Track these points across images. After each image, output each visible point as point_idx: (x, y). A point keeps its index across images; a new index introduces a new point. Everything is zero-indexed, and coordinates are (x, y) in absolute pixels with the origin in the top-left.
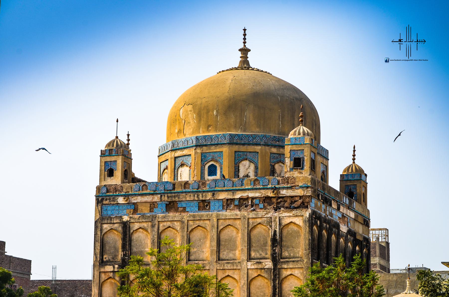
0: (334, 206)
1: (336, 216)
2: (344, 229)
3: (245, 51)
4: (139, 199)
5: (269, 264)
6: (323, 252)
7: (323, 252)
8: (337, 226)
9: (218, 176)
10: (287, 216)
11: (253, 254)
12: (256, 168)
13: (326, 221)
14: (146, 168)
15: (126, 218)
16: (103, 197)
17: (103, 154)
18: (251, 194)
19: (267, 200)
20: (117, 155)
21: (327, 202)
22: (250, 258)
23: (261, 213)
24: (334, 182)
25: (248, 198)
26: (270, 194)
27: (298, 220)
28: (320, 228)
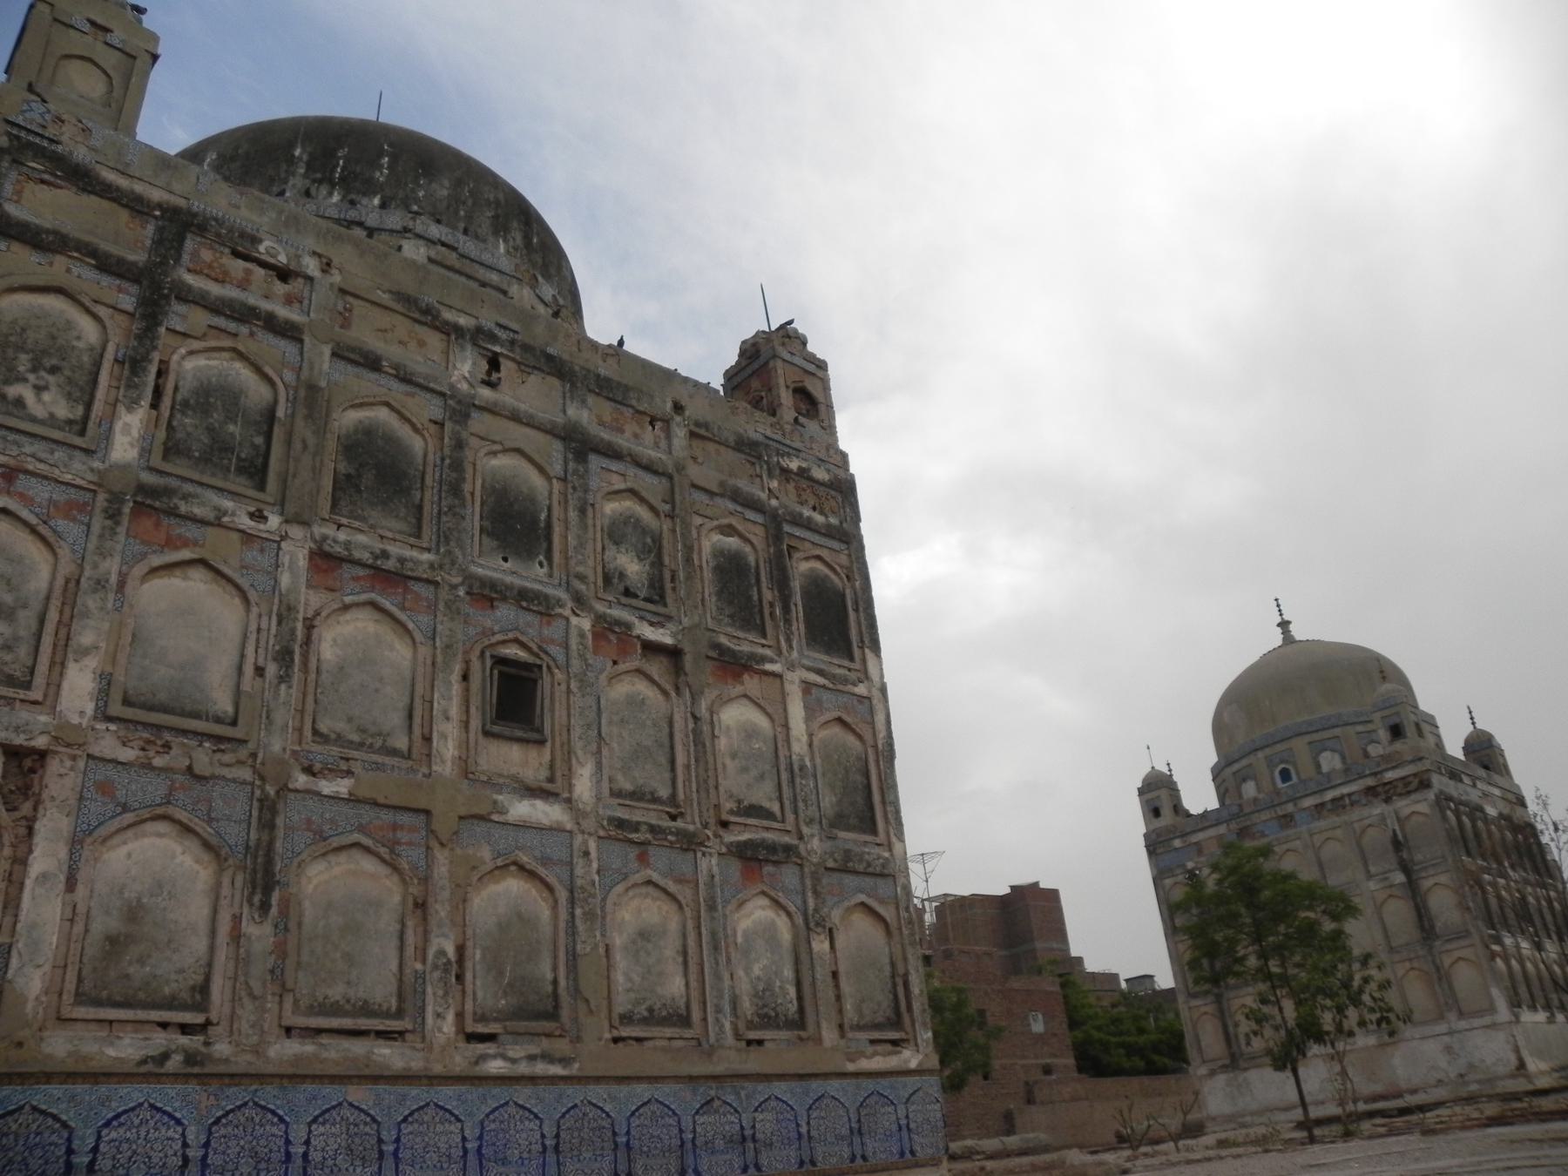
0: (1466, 780)
1: (1474, 796)
2: (1491, 811)
3: (1284, 625)
4: (1200, 836)
5: (1400, 878)
6: (1473, 845)
7: (1473, 845)
8: (1482, 810)
9: (1295, 779)
10: (1404, 806)
11: (1373, 869)
12: (1343, 758)
13: (1466, 804)
14: (1199, 796)
15: (1190, 865)
16: (1155, 844)
17: (1141, 792)
18: (1345, 790)
19: (1371, 791)
20: (1158, 793)
21: (1454, 775)
22: (1370, 876)
23: (1365, 812)
24: (1454, 747)
25: (1342, 797)
26: (1370, 782)
27: (1418, 806)
28: (1457, 814)
